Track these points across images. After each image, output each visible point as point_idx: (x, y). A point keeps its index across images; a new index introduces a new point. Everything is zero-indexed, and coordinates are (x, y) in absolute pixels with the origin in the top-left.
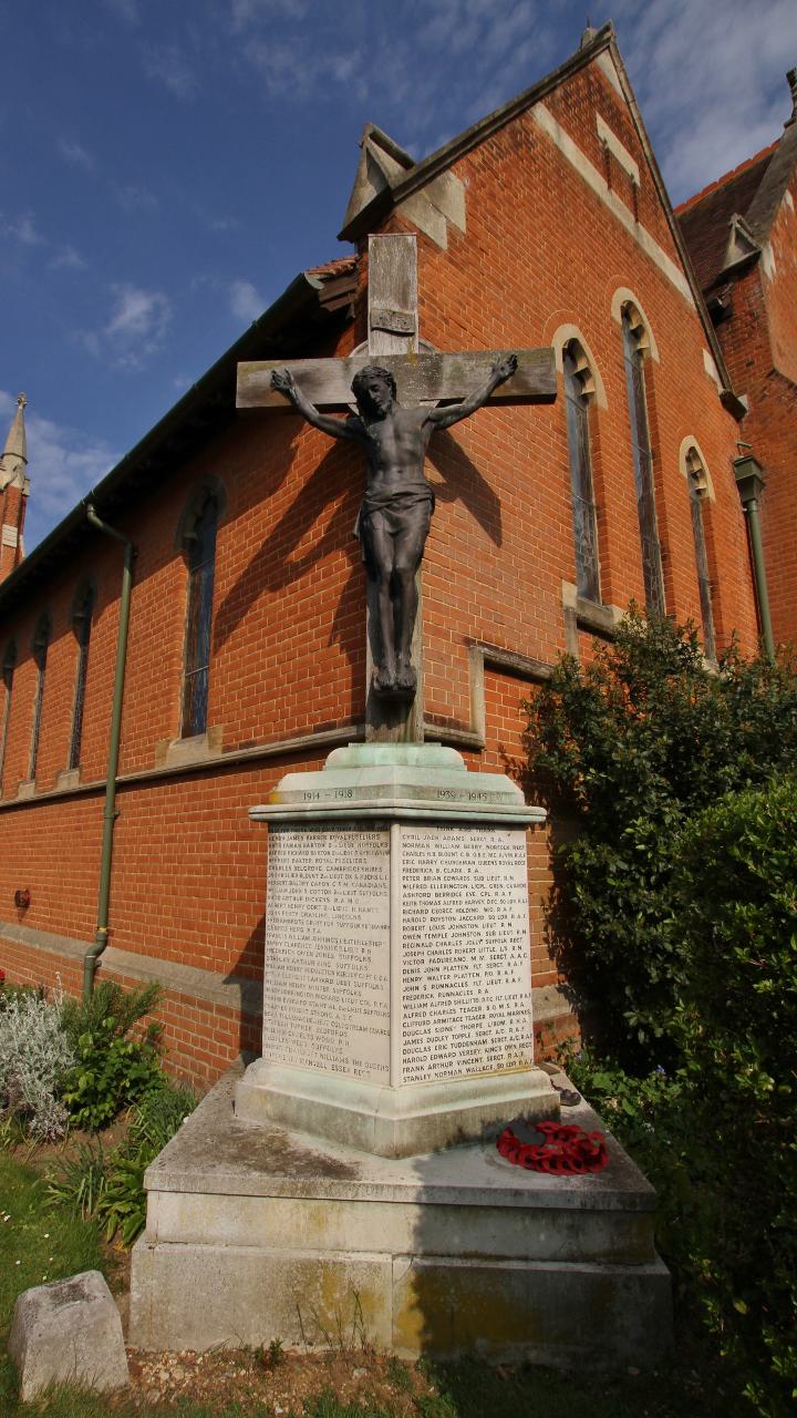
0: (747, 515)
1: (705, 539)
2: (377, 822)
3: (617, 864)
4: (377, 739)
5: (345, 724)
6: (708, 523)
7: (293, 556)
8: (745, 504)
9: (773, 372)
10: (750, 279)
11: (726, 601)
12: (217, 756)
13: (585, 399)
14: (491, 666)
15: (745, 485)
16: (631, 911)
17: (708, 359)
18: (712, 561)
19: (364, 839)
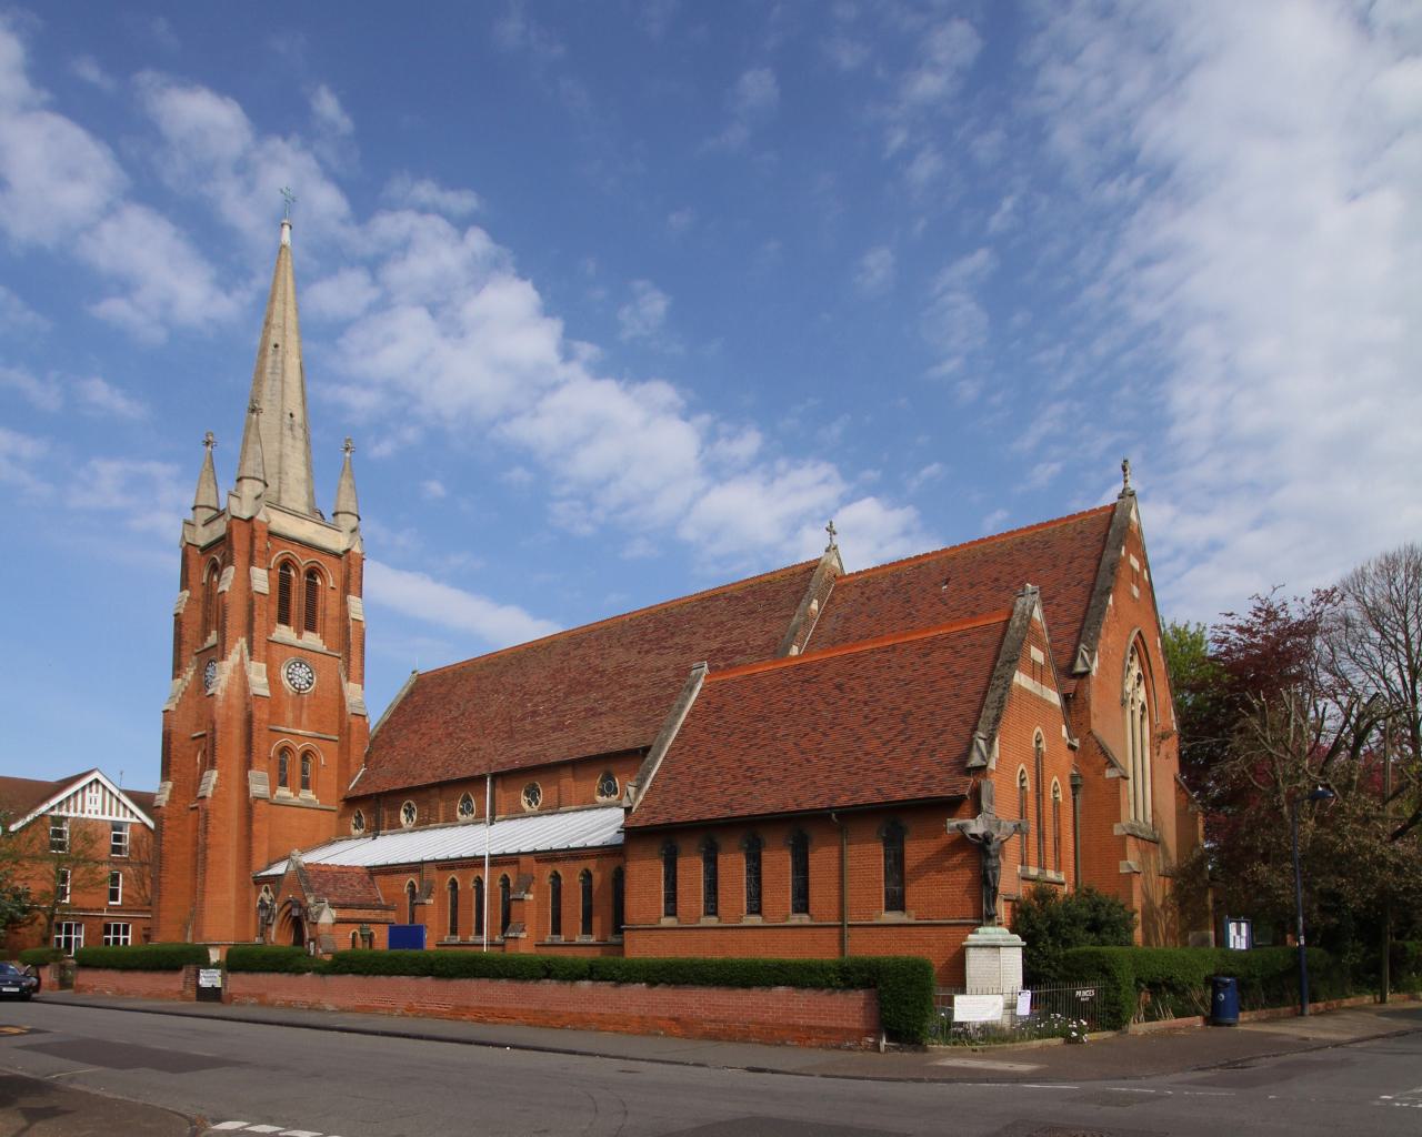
0: (1074, 800)
1: (1057, 819)
2: (999, 947)
3: (1035, 954)
4: (987, 925)
5: (974, 918)
6: (1059, 812)
7: (947, 864)
8: (1074, 795)
9: (1090, 733)
10: (1085, 680)
11: (1063, 845)
12: (913, 921)
13: (1022, 788)
14: (1005, 900)
15: (1074, 787)
16: (1038, 965)
17: (1064, 728)
18: (1059, 829)
19: (993, 950)
